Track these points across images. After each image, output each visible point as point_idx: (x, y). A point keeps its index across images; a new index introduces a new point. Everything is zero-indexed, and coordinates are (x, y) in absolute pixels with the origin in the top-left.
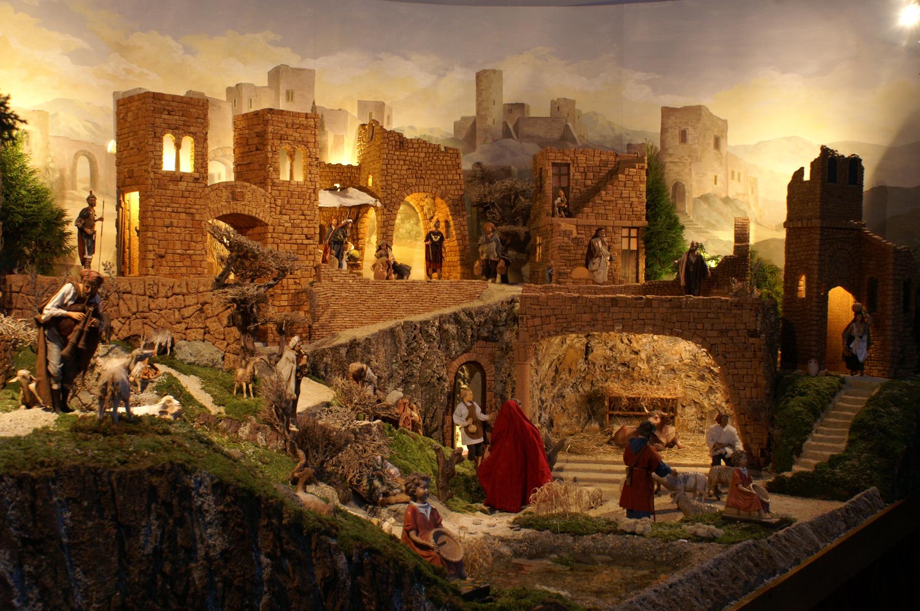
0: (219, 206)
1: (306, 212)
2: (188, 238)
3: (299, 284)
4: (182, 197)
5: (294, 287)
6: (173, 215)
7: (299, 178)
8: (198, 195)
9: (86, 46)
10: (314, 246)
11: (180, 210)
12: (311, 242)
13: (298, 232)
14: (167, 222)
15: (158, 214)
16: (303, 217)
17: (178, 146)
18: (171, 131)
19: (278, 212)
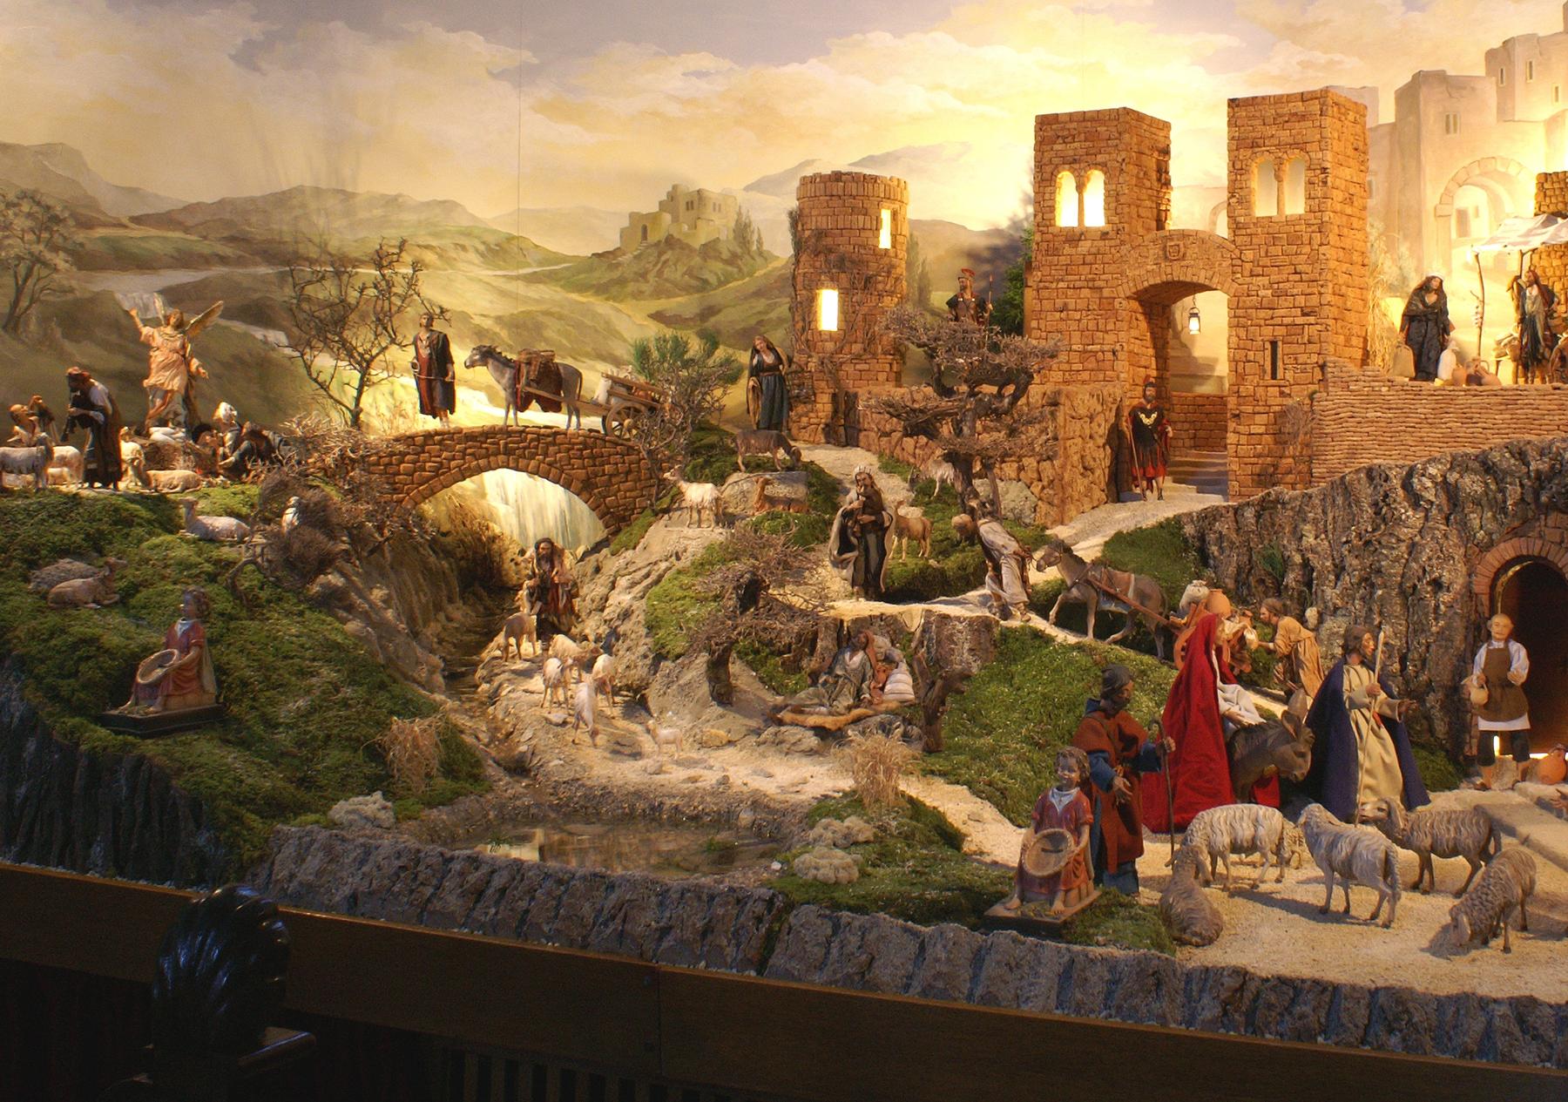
0: (1143, 272)
1: (1299, 268)
2: (1092, 325)
3: (1289, 395)
4: (1084, 264)
5: (1279, 400)
6: (1070, 292)
7: (1096, 218)
8: (1107, 258)
9: (1234, 42)
10: (1319, 327)
11: (1078, 284)
12: (1312, 319)
13: (1287, 305)
14: (1059, 303)
15: (1045, 293)
16: (1297, 277)
17: (1080, 188)
18: (1067, 166)
19: (1247, 273)
